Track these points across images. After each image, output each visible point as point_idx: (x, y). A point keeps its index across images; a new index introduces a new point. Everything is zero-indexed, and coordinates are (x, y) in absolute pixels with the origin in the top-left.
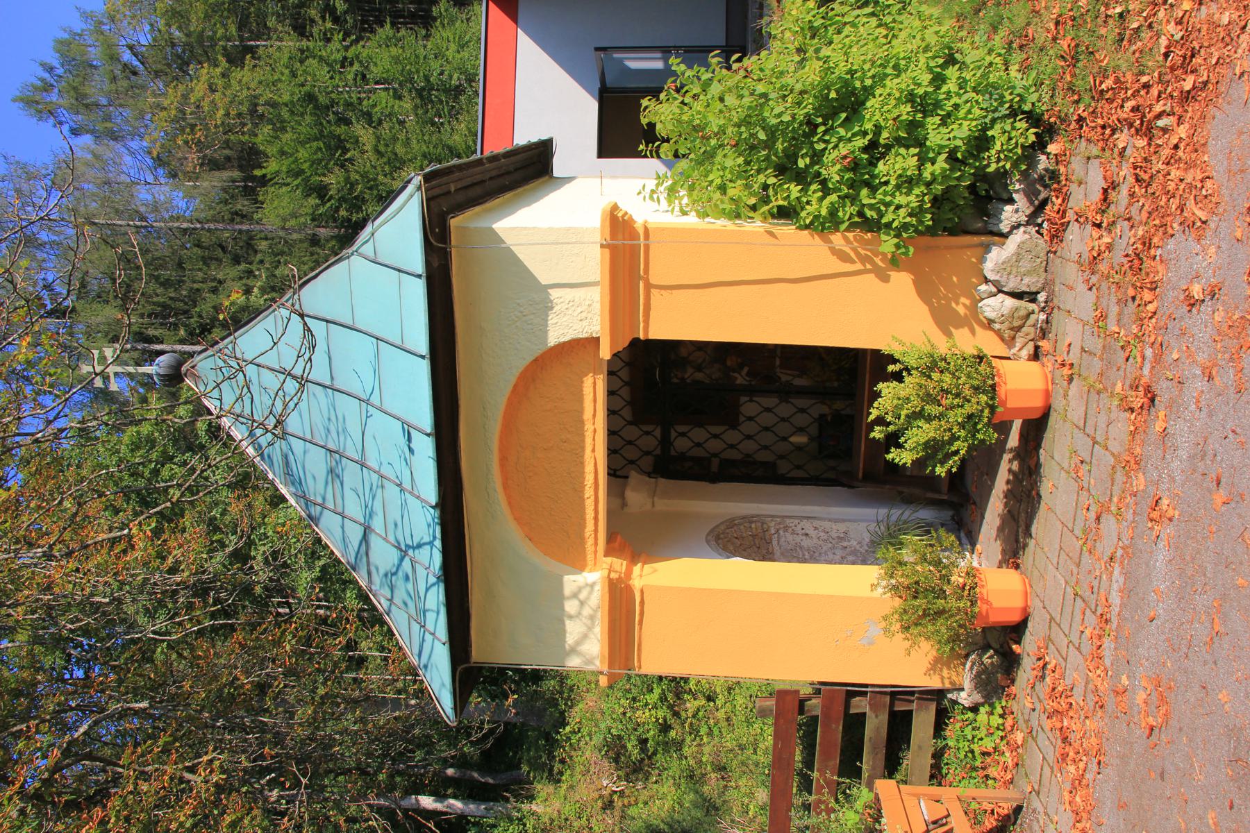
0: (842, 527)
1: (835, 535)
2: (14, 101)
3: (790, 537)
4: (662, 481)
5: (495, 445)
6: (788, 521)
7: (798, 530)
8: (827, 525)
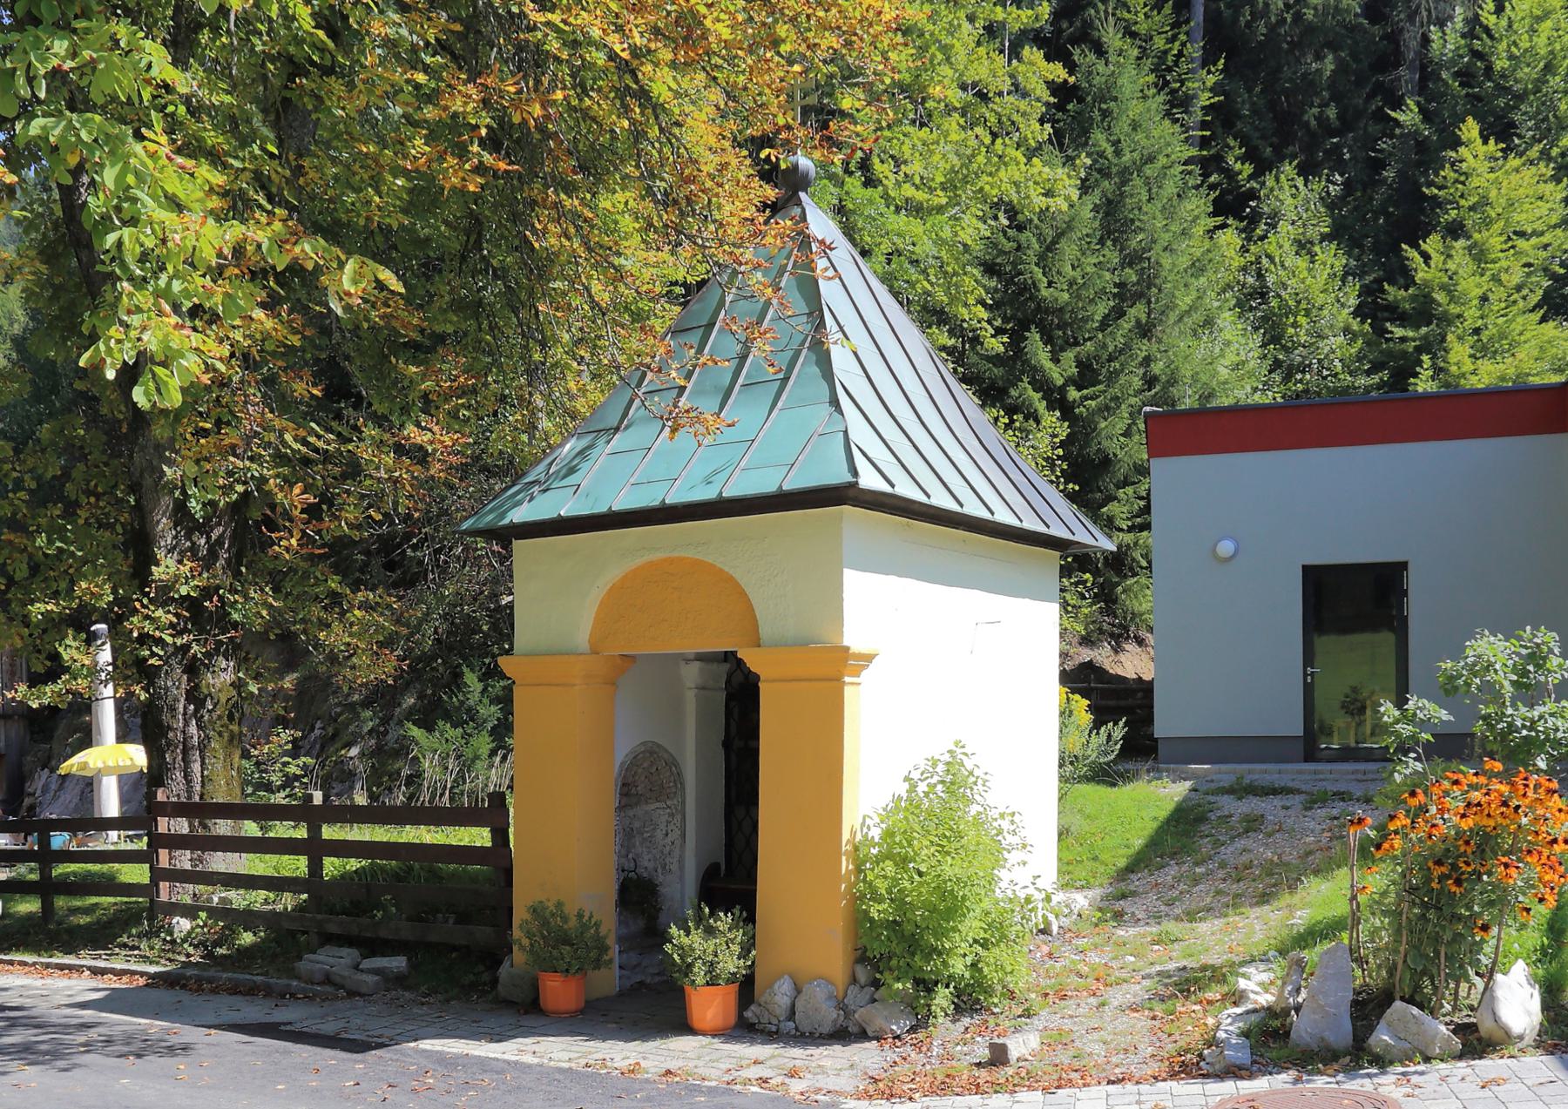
0: (674, 867)
1: (667, 860)
2: (869, 658)
3: (664, 818)
4: (722, 697)
5: (90, 867)
6: (679, 817)
7: (671, 827)
8: (677, 852)
